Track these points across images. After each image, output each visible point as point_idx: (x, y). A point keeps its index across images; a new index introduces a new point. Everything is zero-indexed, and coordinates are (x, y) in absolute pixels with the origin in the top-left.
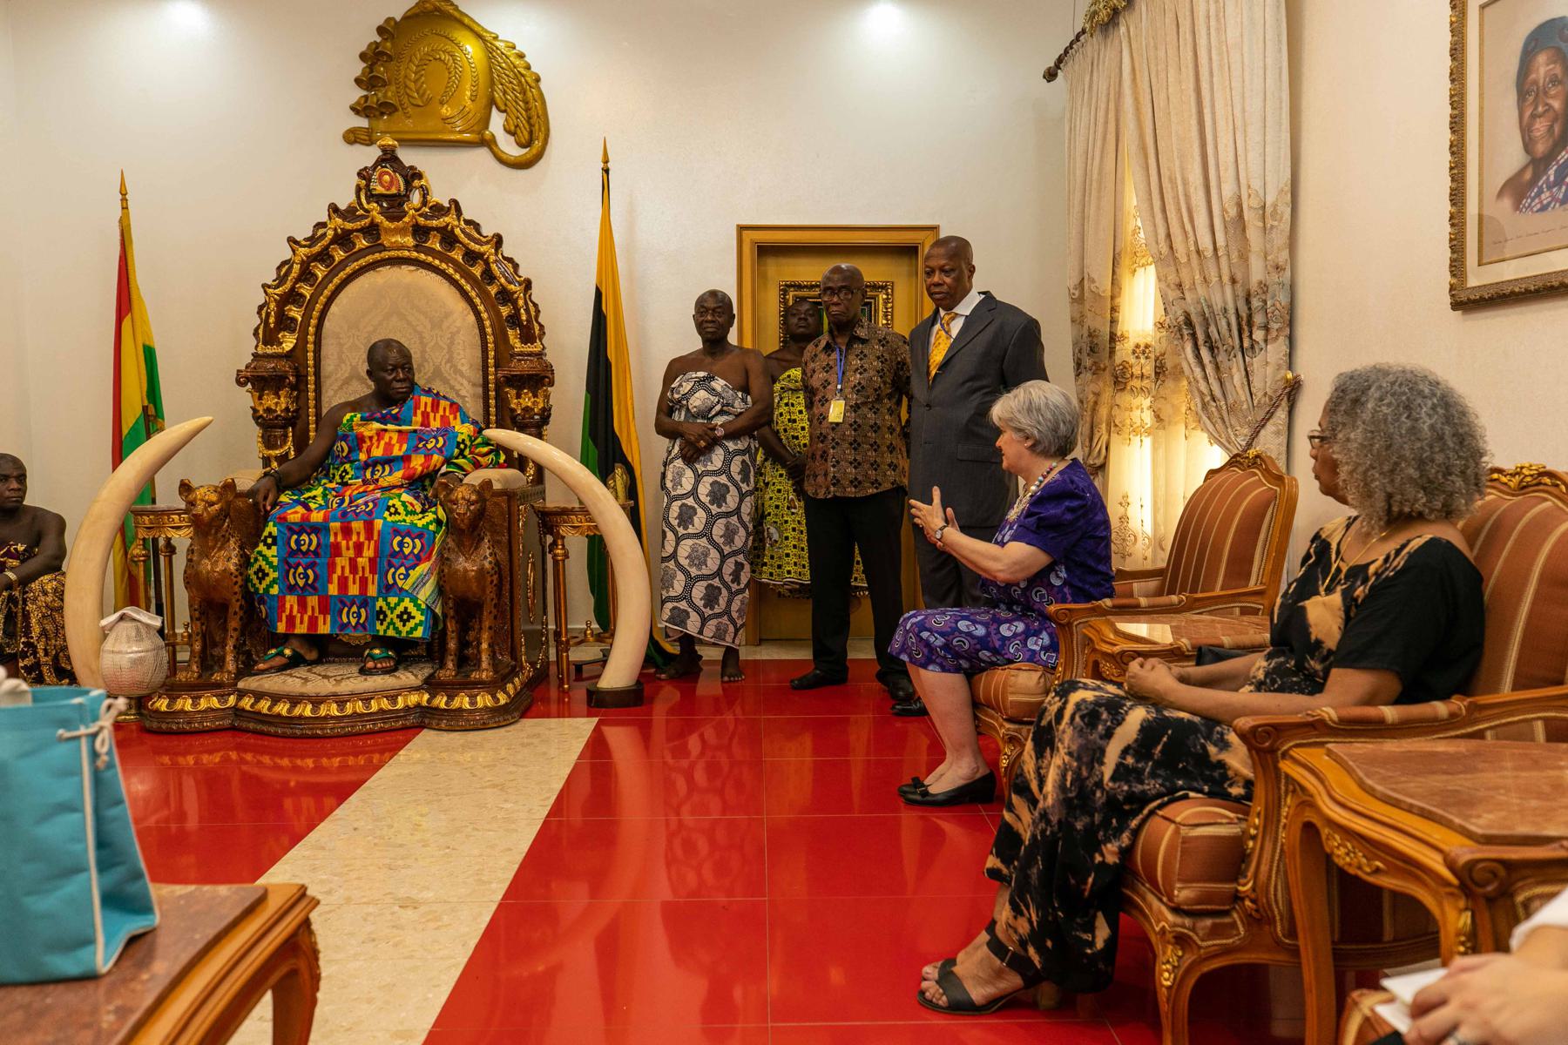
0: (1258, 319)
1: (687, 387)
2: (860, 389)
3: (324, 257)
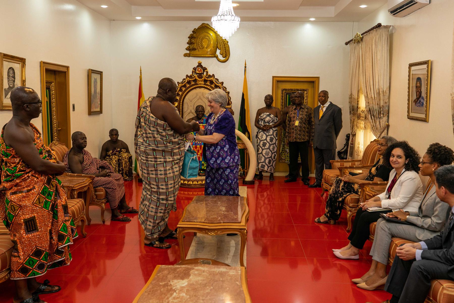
0: (382, 112)
1: (265, 116)
2: (301, 119)
3: (185, 86)
